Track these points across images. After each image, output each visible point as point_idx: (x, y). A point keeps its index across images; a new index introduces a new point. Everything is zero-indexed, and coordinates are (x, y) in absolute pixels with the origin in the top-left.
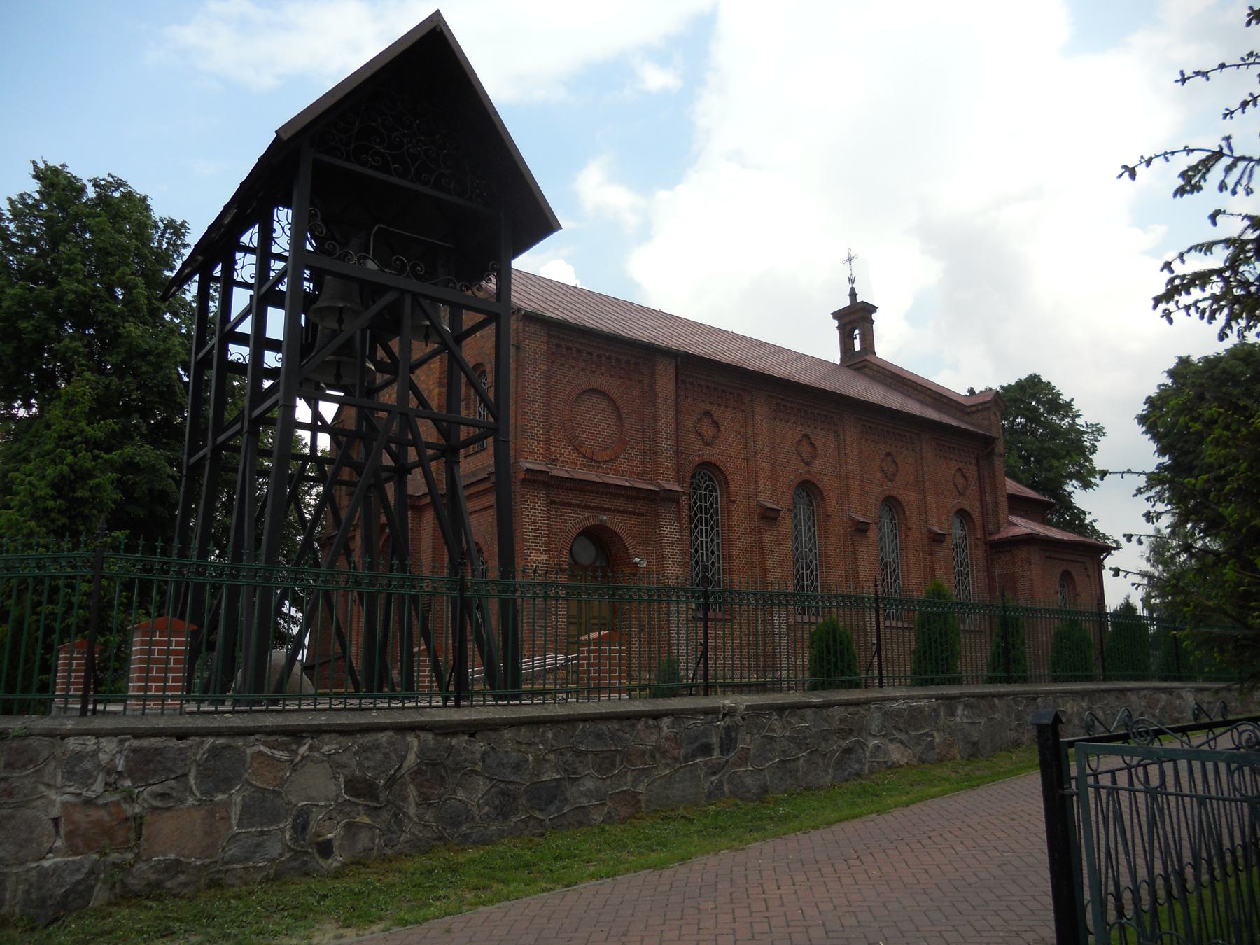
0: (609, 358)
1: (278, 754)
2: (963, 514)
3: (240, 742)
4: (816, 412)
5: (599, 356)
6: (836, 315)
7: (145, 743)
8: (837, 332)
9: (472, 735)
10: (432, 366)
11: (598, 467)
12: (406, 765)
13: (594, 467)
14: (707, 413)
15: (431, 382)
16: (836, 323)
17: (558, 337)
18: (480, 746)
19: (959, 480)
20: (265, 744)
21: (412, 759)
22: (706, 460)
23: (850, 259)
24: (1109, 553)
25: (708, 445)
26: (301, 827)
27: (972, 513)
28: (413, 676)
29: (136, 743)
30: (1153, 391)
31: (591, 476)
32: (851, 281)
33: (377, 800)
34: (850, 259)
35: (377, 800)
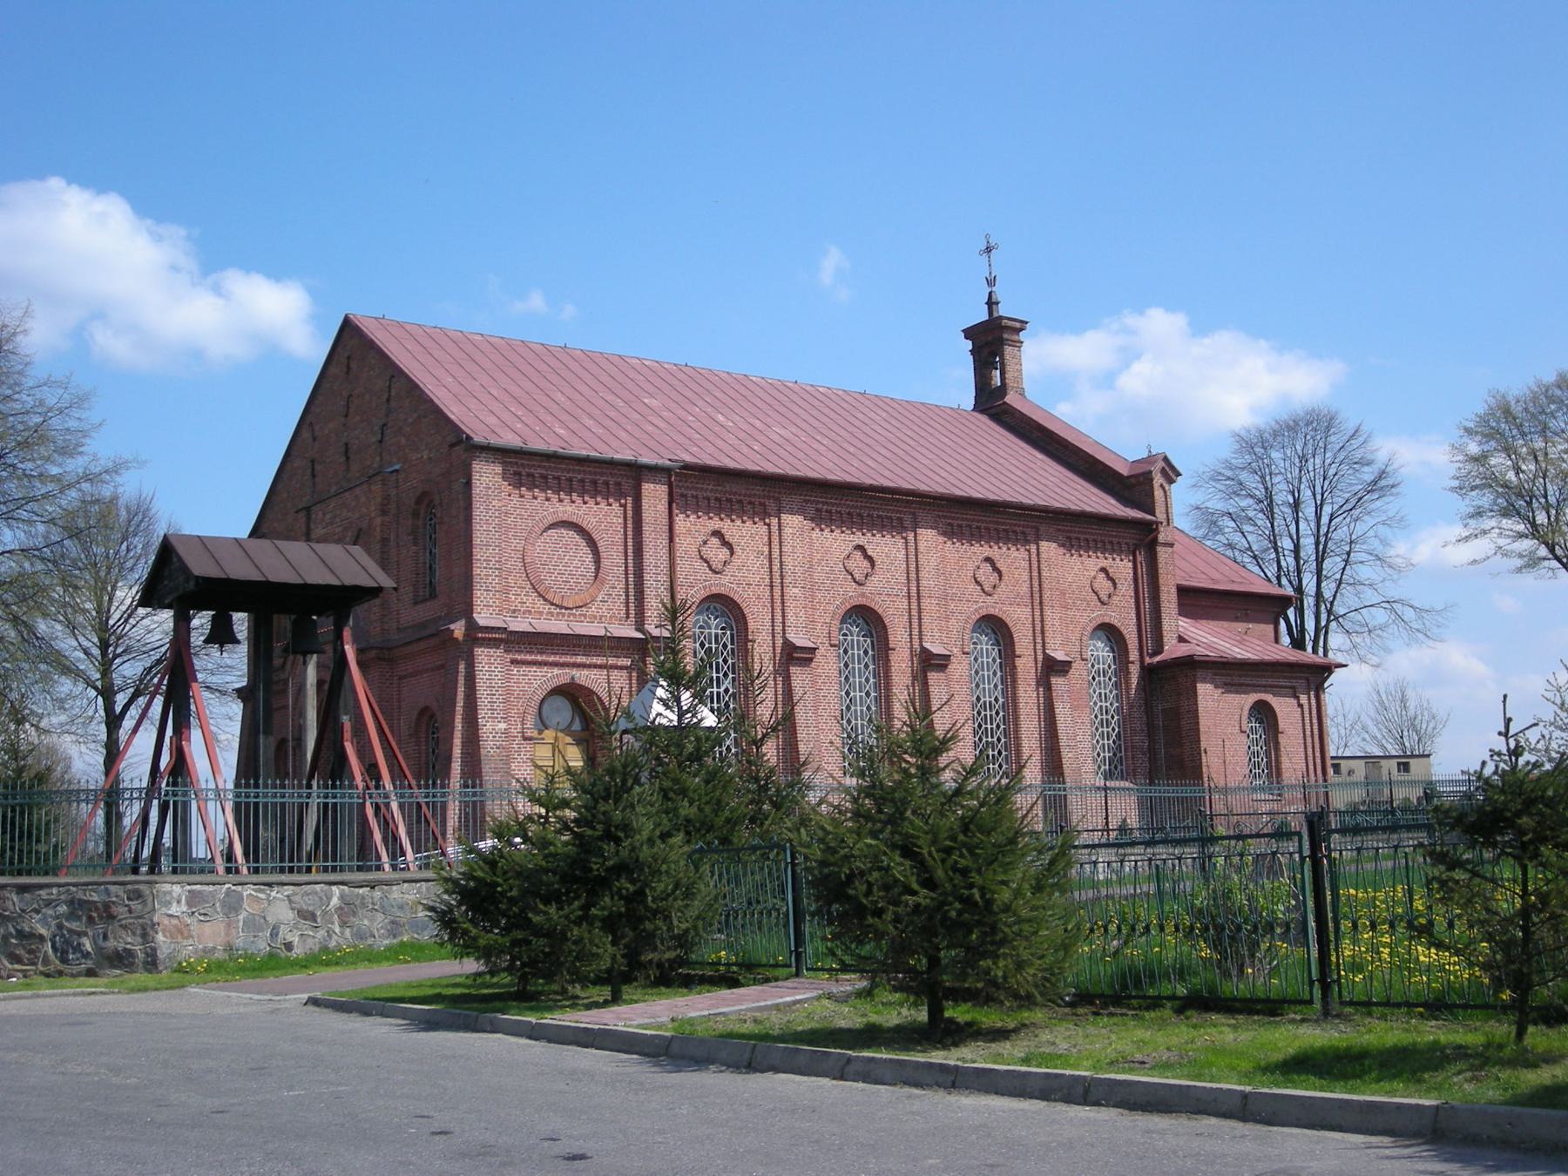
0: (582, 481)
1: (260, 895)
2: (1109, 632)
3: (239, 888)
4: (875, 513)
5: (570, 480)
6: (969, 333)
7: (194, 887)
8: (971, 357)
9: (373, 888)
10: (373, 488)
11: (569, 615)
12: (332, 904)
13: (564, 615)
14: (717, 534)
15: (373, 508)
16: (969, 345)
17: (517, 463)
18: (377, 894)
19: (1103, 584)
20: (253, 890)
21: (335, 901)
22: (715, 592)
23: (989, 250)
24: (1331, 673)
25: (717, 573)
26: (274, 934)
27: (1122, 629)
28: (168, 686)
29: (188, 887)
30: (1481, 411)
31: (559, 626)
32: (991, 282)
33: (316, 922)
34: (989, 250)
35: (316, 922)
